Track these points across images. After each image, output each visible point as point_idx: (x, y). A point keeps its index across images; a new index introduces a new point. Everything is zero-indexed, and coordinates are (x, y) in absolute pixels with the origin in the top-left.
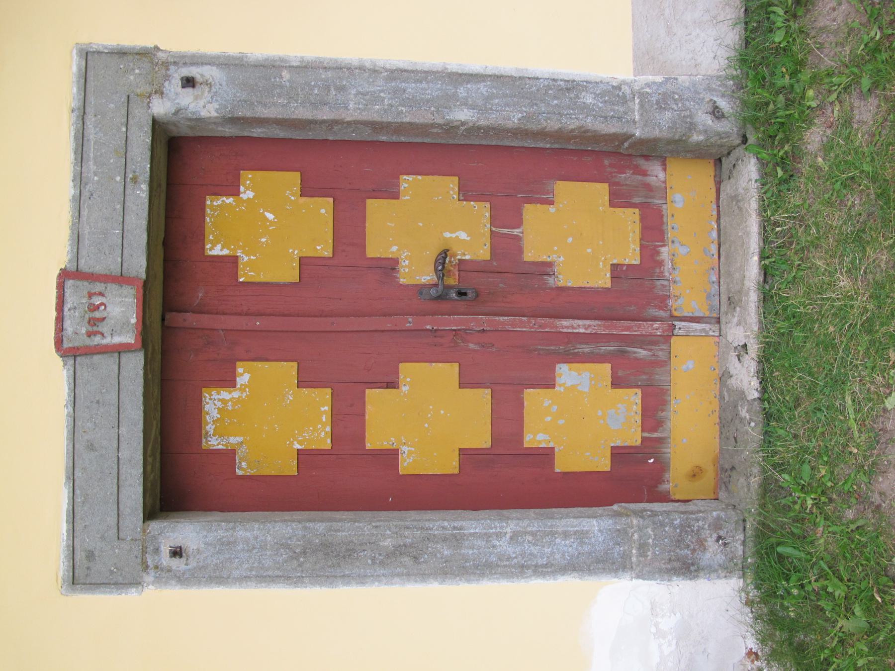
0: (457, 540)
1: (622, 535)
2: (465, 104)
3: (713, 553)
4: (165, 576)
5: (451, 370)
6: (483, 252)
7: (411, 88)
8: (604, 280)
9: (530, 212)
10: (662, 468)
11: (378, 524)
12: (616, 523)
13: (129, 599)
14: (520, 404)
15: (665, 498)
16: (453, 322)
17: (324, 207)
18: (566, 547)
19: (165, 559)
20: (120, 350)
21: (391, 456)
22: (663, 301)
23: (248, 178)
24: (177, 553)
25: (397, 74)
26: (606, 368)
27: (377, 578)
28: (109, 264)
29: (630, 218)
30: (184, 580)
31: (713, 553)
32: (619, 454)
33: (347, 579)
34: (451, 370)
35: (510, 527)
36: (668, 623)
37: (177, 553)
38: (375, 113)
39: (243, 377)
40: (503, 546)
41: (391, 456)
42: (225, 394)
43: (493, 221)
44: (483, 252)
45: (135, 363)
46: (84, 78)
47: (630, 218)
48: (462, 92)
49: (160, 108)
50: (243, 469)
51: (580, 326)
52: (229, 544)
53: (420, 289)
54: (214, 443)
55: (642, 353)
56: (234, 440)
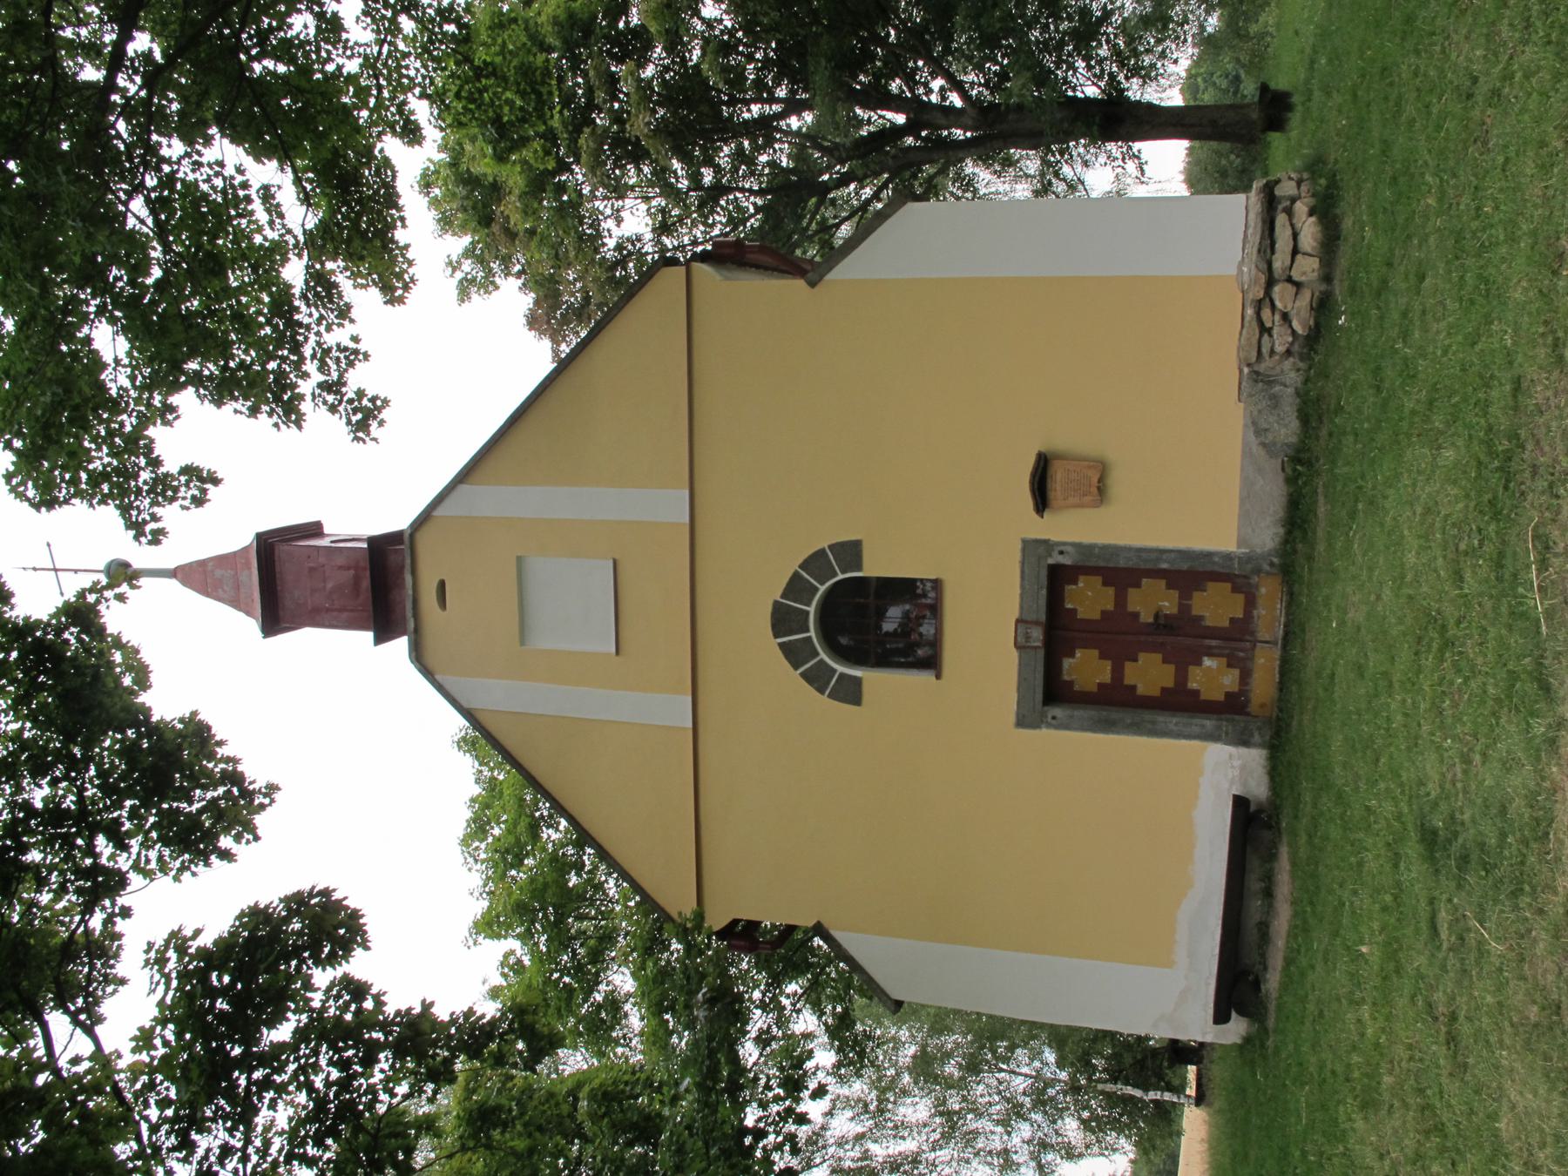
0: (1153, 723)
1: (1219, 728)
2: (1165, 561)
3: (1257, 738)
4: (1049, 726)
5: (1159, 657)
6: (1175, 611)
7: (1144, 555)
8: (1226, 624)
9: (1196, 595)
10: (1248, 701)
11: (143, 859)
12: (1071, 717)
13: (1037, 732)
14: (1187, 671)
15: (1248, 714)
16: (1160, 639)
17: (1111, 591)
18: (1196, 730)
19: (1049, 720)
20: (1036, 648)
21: (1134, 688)
22: (1253, 633)
23: (1082, 578)
24: (1054, 718)
25: (1140, 550)
26: (1225, 660)
27: (1124, 733)
28: (1031, 617)
29: (1240, 598)
30: (1057, 727)
31: (1257, 738)
32: (1228, 695)
33: (1113, 732)
34: (1159, 657)
35: (1174, 720)
36: (1237, 763)
37: (1054, 718)
38: (1130, 564)
39: (1078, 654)
40: (1172, 726)
41: (1134, 688)
42: (1071, 660)
43: (1180, 598)
44: (1175, 611)
45: (1041, 653)
46: (1023, 550)
47: (1240, 598)
48: (1164, 557)
49: (1050, 561)
50: (1076, 688)
51: (1214, 643)
52: (1071, 717)
53: (1149, 624)
54: (1066, 677)
55: (1241, 654)
56: (1074, 677)
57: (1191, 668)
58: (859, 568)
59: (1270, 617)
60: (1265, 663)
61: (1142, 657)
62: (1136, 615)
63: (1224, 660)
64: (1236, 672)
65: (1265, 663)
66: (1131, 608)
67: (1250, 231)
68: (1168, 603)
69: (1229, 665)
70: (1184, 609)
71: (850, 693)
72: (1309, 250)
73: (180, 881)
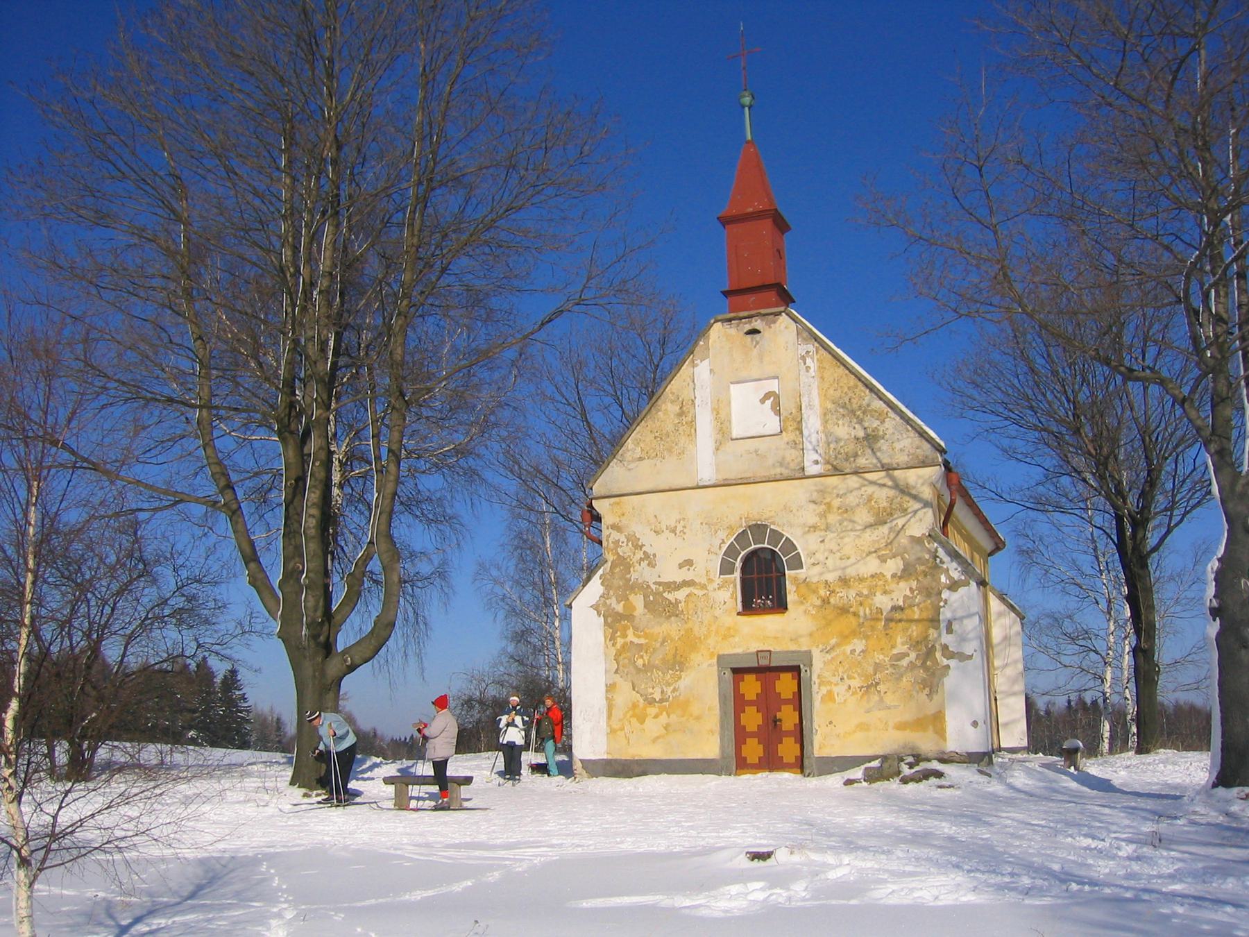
71: (726, 569)
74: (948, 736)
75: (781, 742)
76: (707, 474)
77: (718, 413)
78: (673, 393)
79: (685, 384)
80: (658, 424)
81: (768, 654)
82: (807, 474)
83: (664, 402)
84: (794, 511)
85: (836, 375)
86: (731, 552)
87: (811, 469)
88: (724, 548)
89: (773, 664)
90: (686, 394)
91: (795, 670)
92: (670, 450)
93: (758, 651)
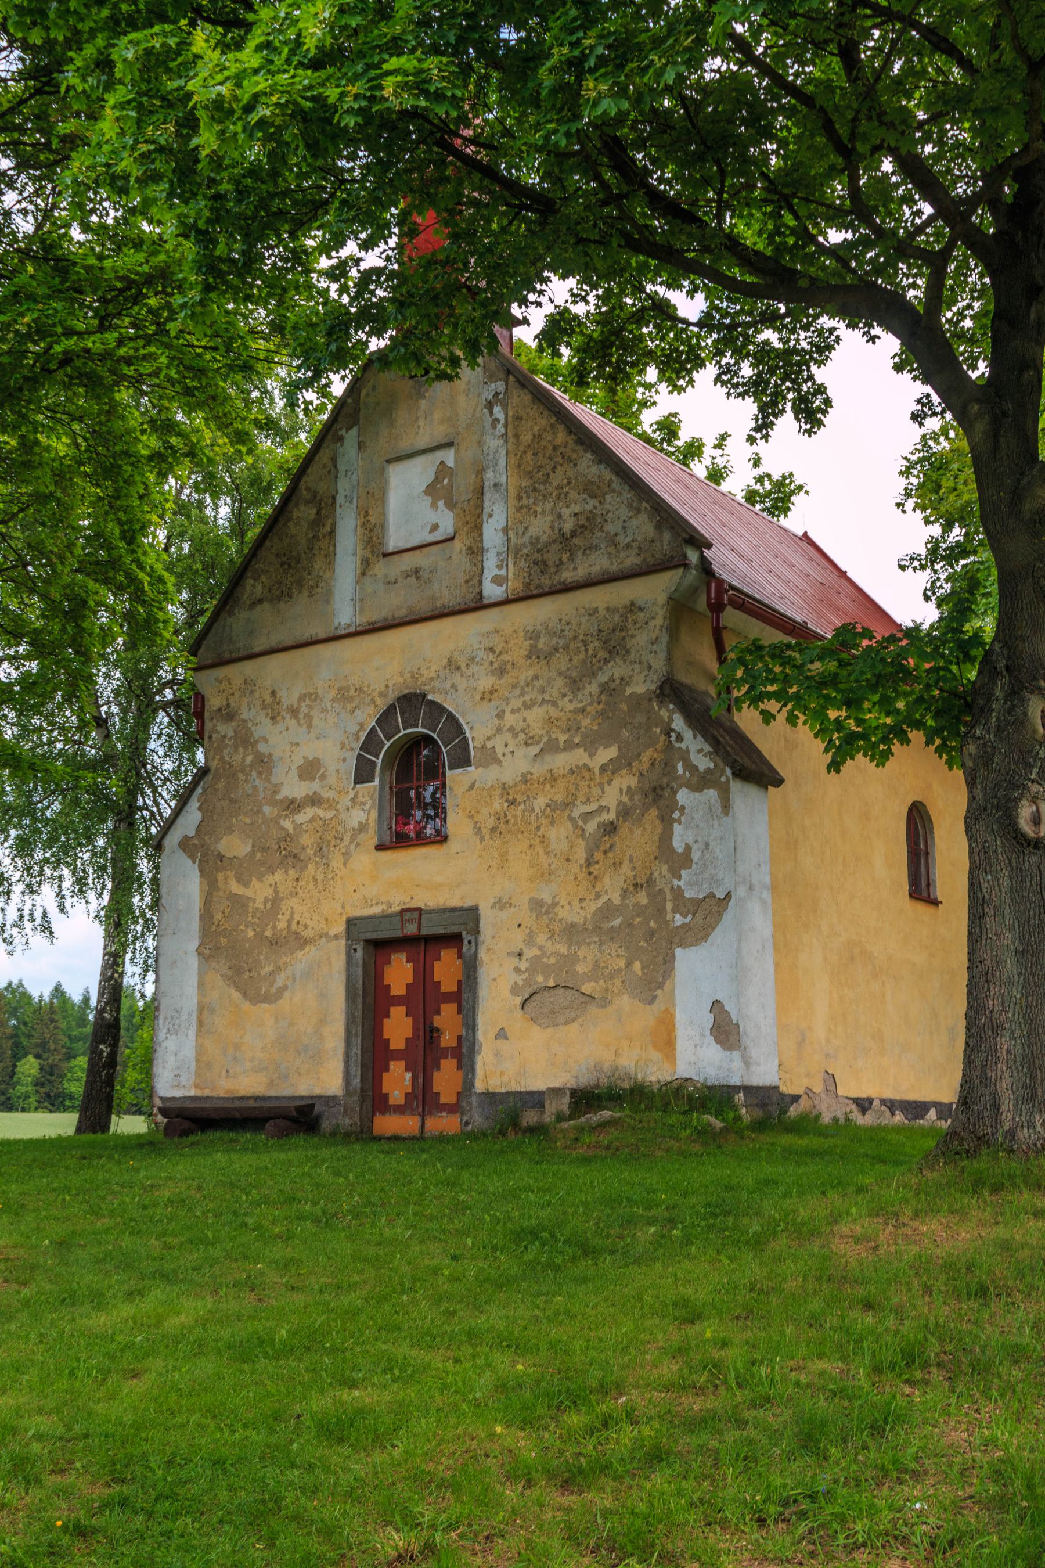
16: (421, 1034)
22: (430, 1113)
44: (443, 1045)
49: (464, 933)
51: (421, 1080)
57: (403, 1063)
58: (450, 769)
59: (443, 1123)
60: (407, 1124)
61: (410, 1020)
62: (438, 1012)
63: (410, 1090)
64: (402, 1102)
65: (407, 1124)
66: (443, 1006)
67: (352, 1064)
68: (447, 1040)
69: (407, 1095)
70: (445, 1053)
71: (363, 775)
72: (427, 1125)
73: (692, 298)
74: (678, 1054)
75: (388, 1016)
76: (345, 616)
77: (367, 514)
78: (308, 489)
79: (325, 471)
80: (286, 541)
81: (416, 914)
82: (486, 601)
83: (297, 505)
84: (463, 668)
85: (536, 428)
86: (370, 744)
87: (492, 591)
88: (363, 736)
89: (424, 932)
90: (322, 487)
91: (453, 939)
92: (300, 584)
93: (403, 911)
